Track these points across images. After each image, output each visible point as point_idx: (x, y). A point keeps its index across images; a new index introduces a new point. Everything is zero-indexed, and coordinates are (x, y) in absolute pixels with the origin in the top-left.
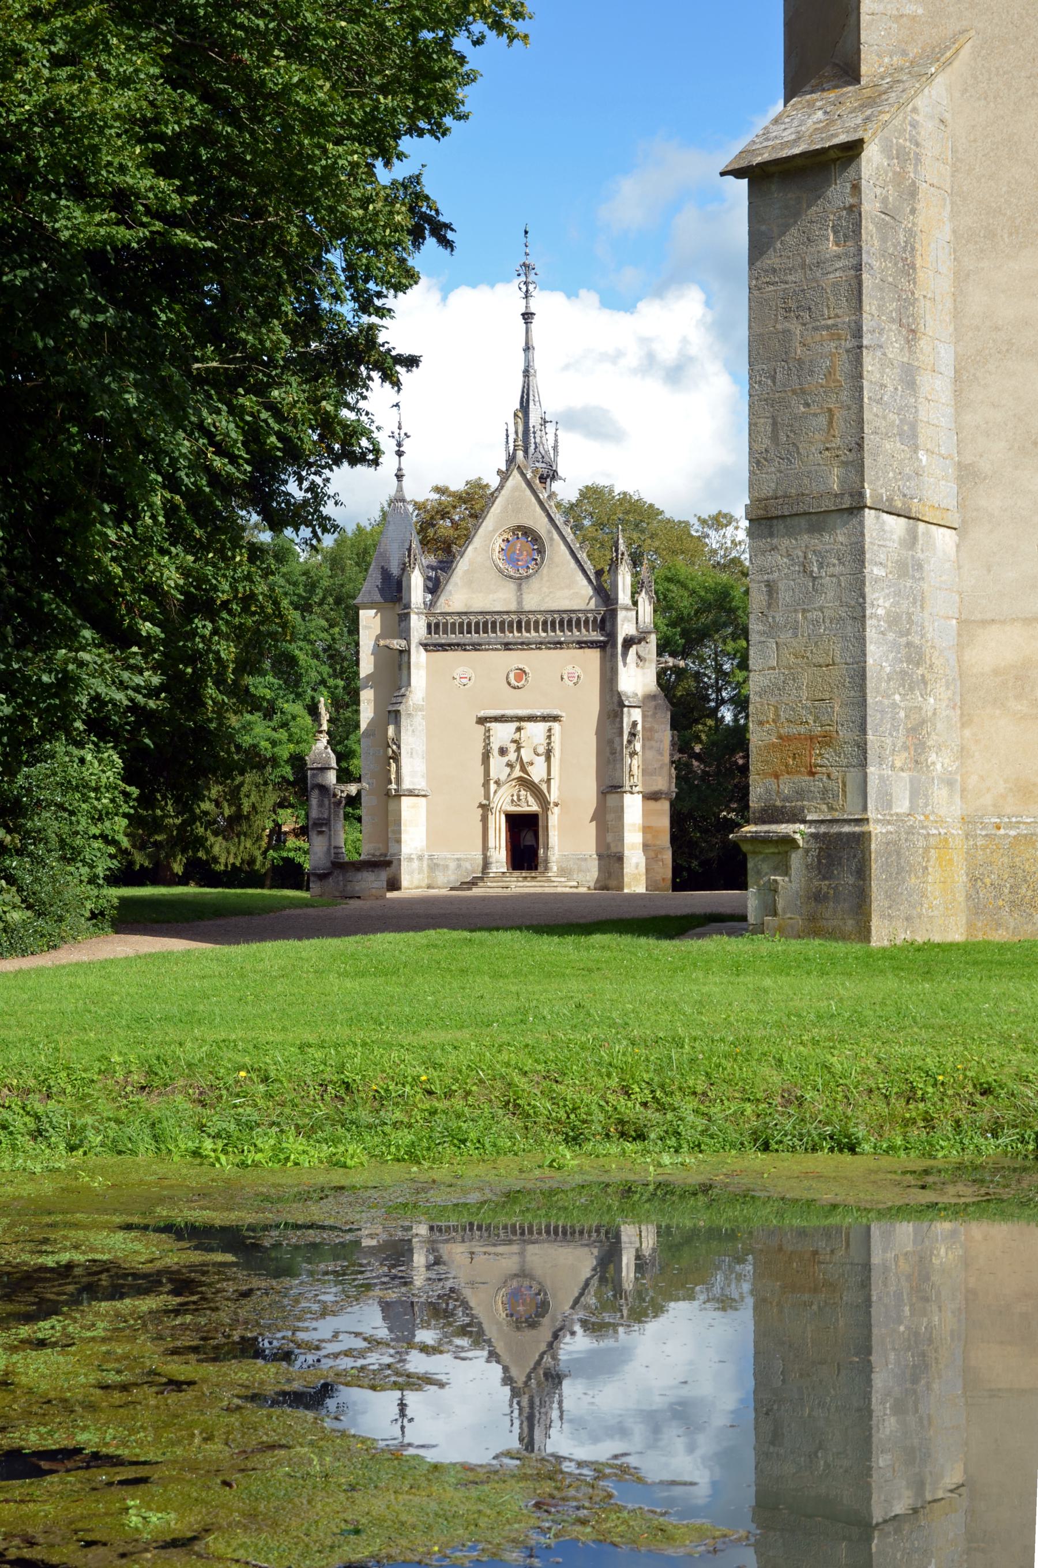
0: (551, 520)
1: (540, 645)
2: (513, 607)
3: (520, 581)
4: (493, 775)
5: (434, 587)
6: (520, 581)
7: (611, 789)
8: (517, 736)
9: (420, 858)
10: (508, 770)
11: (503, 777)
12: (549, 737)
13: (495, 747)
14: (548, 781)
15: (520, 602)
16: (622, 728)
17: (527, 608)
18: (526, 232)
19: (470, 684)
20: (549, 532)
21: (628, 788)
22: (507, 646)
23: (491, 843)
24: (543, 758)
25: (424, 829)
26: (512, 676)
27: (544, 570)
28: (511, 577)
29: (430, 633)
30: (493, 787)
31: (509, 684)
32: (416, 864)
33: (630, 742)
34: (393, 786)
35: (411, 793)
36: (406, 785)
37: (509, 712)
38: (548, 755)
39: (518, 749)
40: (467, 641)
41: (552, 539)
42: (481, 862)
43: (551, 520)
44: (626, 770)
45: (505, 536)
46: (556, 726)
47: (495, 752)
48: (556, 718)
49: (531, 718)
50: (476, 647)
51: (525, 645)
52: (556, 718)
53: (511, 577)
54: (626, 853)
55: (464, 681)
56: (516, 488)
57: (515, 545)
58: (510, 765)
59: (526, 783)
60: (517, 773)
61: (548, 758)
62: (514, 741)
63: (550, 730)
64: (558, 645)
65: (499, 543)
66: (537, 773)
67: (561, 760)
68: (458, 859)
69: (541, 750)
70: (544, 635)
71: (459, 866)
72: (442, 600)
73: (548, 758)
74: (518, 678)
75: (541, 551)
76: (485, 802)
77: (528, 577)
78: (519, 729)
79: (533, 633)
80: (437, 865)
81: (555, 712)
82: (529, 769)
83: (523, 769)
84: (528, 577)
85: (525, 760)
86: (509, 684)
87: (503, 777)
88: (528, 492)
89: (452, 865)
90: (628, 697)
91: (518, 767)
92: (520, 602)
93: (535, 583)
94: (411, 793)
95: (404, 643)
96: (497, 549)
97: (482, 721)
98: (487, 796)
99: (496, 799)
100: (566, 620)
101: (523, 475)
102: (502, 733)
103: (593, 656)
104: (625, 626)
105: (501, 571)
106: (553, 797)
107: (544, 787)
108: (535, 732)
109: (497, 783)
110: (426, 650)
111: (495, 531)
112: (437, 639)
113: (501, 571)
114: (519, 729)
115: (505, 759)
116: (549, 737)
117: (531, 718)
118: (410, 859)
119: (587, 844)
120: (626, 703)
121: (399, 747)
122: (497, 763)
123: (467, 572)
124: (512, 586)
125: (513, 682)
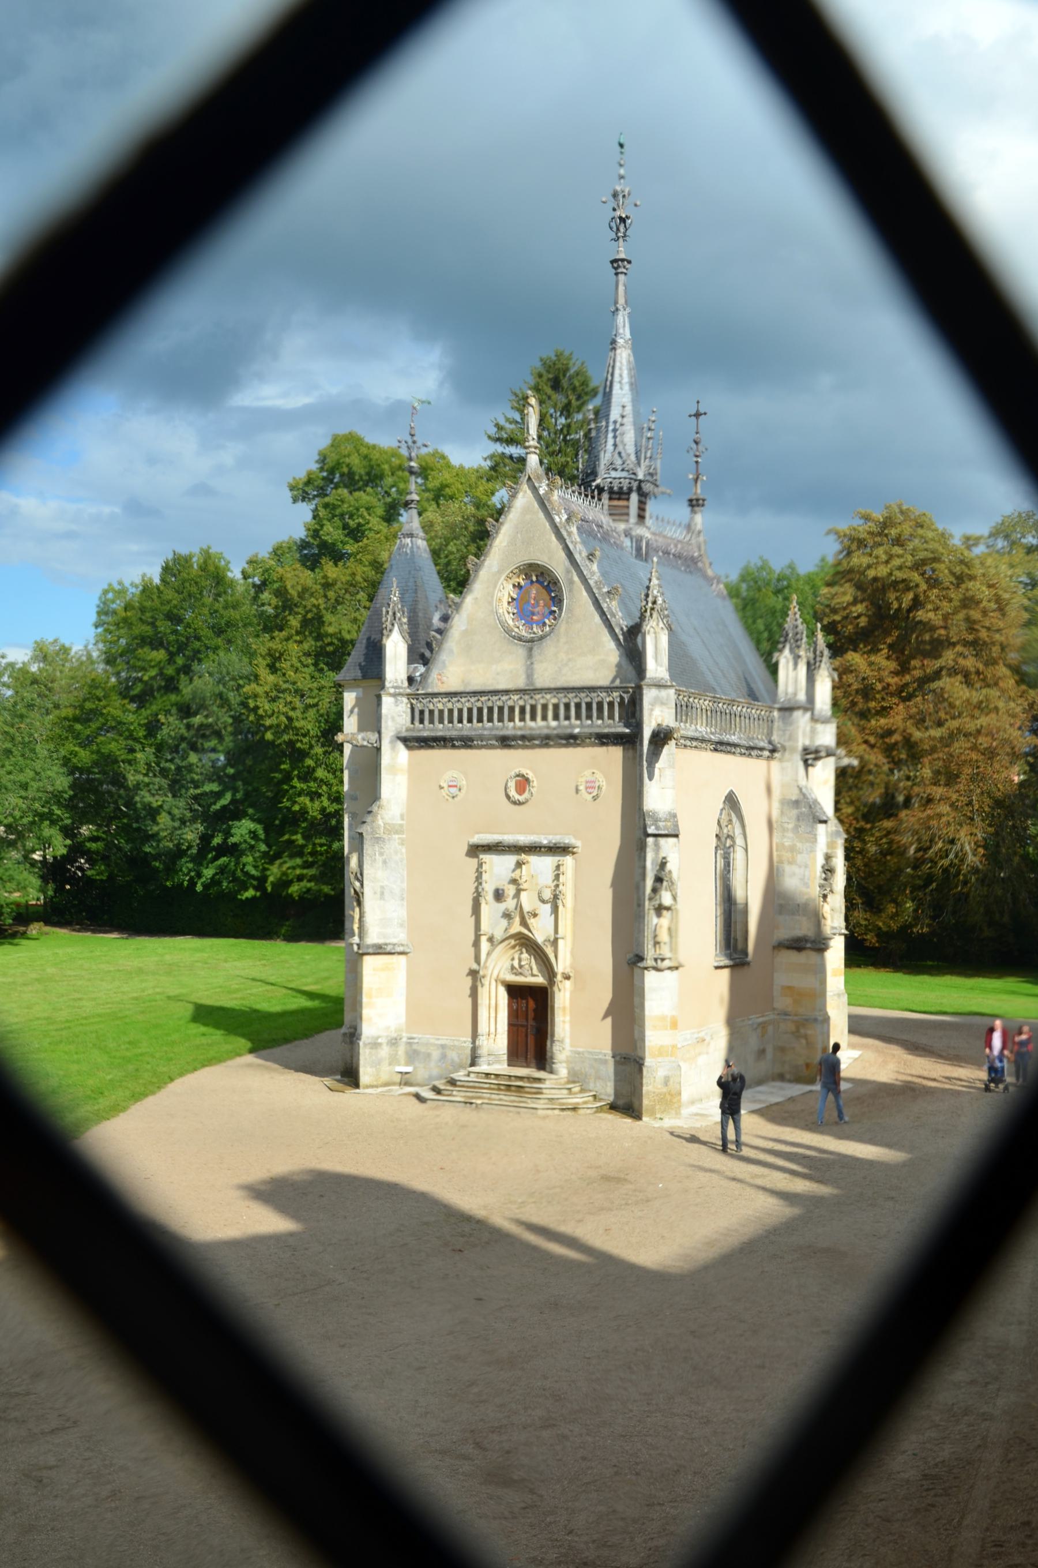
0: (570, 555)
1: (546, 741)
2: (521, 683)
3: (531, 644)
4: (485, 926)
5: (422, 654)
6: (531, 644)
7: (631, 961)
8: (516, 875)
9: (394, 1042)
10: (504, 923)
11: (499, 935)
12: (557, 877)
13: (489, 888)
14: (555, 943)
15: (530, 675)
16: (644, 868)
17: (539, 684)
18: (621, 146)
19: (461, 795)
20: (568, 572)
21: (650, 962)
22: (505, 742)
23: (483, 1027)
24: (548, 906)
25: (402, 1001)
26: (512, 785)
27: (562, 626)
28: (520, 639)
29: (412, 722)
30: (485, 946)
31: (508, 797)
32: (385, 1052)
33: (655, 890)
34: (356, 939)
35: (380, 950)
36: (373, 937)
37: (509, 838)
38: (555, 903)
39: (517, 895)
40: (454, 733)
41: (571, 582)
42: (468, 1052)
43: (570, 555)
44: (648, 934)
45: (515, 580)
46: (568, 861)
47: (489, 896)
48: (560, 850)
49: (534, 849)
50: (467, 742)
51: (526, 741)
52: (560, 850)
53: (520, 639)
54: (649, 1061)
55: (453, 790)
56: (526, 510)
57: (528, 593)
58: (507, 915)
59: (526, 943)
60: (517, 928)
61: (555, 910)
62: (514, 881)
63: (558, 867)
64: (571, 740)
65: (506, 591)
66: (541, 931)
67: (575, 910)
68: (443, 1046)
69: (547, 895)
70: (554, 724)
71: (444, 1056)
72: (434, 675)
73: (555, 910)
74: (521, 790)
75: (558, 601)
76: (475, 966)
77: (542, 638)
78: (519, 865)
79: (540, 722)
80: (416, 1053)
81: (567, 840)
82: (531, 922)
83: (524, 923)
84: (542, 638)
85: (527, 908)
86: (508, 797)
87: (499, 935)
88: (541, 515)
89: (436, 1054)
90: (656, 821)
91: (517, 920)
92: (530, 675)
93: (549, 647)
94: (380, 950)
95: (373, 737)
96: (506, 599)
97: (476, 850)
98: (477, 959)
99: (490, 964)
100: (581, 701)
101: (535, 490)
102: (499, 868)
103: (616, 753)
104: (657, 712)
105: (508, 631)
106: (561, 966)
107: (549, 951)
108: (541, 866)
109: (491, 940)
110: (409, 748)
111: (500, 572)
112: (427, 730)
113: (508, 631)
114: (519, 865)
115: (502, 907)
116: (557, 877)
117: (534, 849)
118: (375, 1045)
119: (600, 1040)
120: (651, 830)
121: (362, 885)
122: (490, 910)
123: (465, 633)
124: (520, 651)
125: (513, 793)
